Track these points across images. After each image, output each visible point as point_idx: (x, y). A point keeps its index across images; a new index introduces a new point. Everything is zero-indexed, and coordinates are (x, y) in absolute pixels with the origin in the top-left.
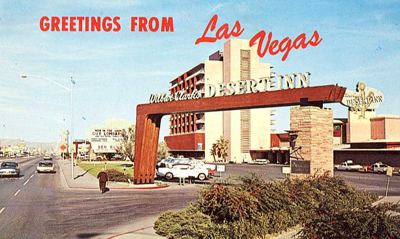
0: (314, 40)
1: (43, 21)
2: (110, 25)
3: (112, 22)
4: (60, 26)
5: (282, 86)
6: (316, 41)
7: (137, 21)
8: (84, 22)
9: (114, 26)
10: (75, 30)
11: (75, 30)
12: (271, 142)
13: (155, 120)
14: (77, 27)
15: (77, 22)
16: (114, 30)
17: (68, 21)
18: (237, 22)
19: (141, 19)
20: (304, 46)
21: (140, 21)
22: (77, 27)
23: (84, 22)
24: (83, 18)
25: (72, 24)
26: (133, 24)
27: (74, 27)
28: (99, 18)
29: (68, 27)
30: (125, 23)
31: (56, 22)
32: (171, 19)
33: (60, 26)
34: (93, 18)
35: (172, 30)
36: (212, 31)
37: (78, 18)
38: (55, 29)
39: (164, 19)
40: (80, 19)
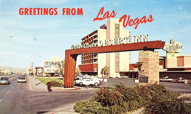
0: (150, 19)
1: (20, 10)
2: (53, 12)
3: (53, 10)
4: (29, 12)
5: (135, 41)
6: (151, 20)
7: (65, 10)
8: (40, 10)
9: (54, 12)
10: (36, 14)
11: (36, 14)
12: (129, 68)
13: (74, 57)
14: (37, 13)
15: (37, 10)
16: (55, 14)
17: (33, 10)
18: (113, 11)
19: (67, 9)
20: (145, 22)
21: (67, 10)
22: (37, 13)
23: (40, 10)
24: (40, 9)
25: (35, 11)
26: (64, 12)
27: (35, 13)
28: (47, 9)
29: (32, 13)
30: (60, 11)
31: (27, 10)
32: (81, 9)
33: (29, 12)
34: (44, 9)
35: (82, 14)
36: (101, 15)
37: (37, 9)
38: (26, 14)
39: (78, 9)
40: (38, 9)
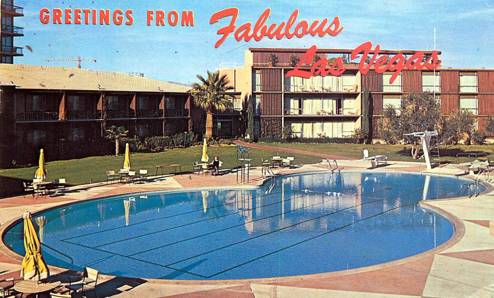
0: (332, 28)
1: (171, 16)
2: (121, 18)
3: (124, 16)
4: (62, 19)
5: (332, 125)
6: (336, 29)
7: (154, 16)
8: (90, 16)
9: (125, 20)
10: (79, 23)
11: (79, 23)
12: (422, 81)
13: (320, 160)
14: (82, 21)
15: (82, 15)
16: (127, 24)
17: (72, 15)
18: (336, 19)
19: (158, 13)
20: (321, 35)
21: (158, 16)
22: (82, 21)
23: (90, 16)
24: (89, 11)
25: (77, 17)
26: (149, 18)
27: (69, 20)
28: (107, 11)
29: (72, 20)
30: (139, 18)
31: (57, 14)
32: (191, 13)
33: (62, 19)
34: (102, 12)
35: (192, 25)
36: (318, 21)
37: (84, 11)
38: (57, 22)
39: (184, 13)
40: (87, 12)
